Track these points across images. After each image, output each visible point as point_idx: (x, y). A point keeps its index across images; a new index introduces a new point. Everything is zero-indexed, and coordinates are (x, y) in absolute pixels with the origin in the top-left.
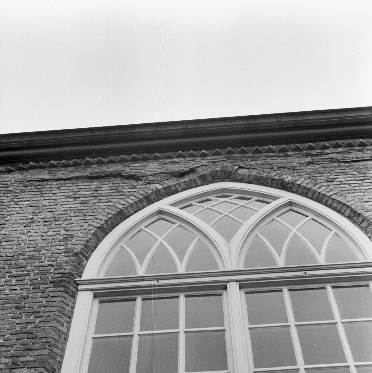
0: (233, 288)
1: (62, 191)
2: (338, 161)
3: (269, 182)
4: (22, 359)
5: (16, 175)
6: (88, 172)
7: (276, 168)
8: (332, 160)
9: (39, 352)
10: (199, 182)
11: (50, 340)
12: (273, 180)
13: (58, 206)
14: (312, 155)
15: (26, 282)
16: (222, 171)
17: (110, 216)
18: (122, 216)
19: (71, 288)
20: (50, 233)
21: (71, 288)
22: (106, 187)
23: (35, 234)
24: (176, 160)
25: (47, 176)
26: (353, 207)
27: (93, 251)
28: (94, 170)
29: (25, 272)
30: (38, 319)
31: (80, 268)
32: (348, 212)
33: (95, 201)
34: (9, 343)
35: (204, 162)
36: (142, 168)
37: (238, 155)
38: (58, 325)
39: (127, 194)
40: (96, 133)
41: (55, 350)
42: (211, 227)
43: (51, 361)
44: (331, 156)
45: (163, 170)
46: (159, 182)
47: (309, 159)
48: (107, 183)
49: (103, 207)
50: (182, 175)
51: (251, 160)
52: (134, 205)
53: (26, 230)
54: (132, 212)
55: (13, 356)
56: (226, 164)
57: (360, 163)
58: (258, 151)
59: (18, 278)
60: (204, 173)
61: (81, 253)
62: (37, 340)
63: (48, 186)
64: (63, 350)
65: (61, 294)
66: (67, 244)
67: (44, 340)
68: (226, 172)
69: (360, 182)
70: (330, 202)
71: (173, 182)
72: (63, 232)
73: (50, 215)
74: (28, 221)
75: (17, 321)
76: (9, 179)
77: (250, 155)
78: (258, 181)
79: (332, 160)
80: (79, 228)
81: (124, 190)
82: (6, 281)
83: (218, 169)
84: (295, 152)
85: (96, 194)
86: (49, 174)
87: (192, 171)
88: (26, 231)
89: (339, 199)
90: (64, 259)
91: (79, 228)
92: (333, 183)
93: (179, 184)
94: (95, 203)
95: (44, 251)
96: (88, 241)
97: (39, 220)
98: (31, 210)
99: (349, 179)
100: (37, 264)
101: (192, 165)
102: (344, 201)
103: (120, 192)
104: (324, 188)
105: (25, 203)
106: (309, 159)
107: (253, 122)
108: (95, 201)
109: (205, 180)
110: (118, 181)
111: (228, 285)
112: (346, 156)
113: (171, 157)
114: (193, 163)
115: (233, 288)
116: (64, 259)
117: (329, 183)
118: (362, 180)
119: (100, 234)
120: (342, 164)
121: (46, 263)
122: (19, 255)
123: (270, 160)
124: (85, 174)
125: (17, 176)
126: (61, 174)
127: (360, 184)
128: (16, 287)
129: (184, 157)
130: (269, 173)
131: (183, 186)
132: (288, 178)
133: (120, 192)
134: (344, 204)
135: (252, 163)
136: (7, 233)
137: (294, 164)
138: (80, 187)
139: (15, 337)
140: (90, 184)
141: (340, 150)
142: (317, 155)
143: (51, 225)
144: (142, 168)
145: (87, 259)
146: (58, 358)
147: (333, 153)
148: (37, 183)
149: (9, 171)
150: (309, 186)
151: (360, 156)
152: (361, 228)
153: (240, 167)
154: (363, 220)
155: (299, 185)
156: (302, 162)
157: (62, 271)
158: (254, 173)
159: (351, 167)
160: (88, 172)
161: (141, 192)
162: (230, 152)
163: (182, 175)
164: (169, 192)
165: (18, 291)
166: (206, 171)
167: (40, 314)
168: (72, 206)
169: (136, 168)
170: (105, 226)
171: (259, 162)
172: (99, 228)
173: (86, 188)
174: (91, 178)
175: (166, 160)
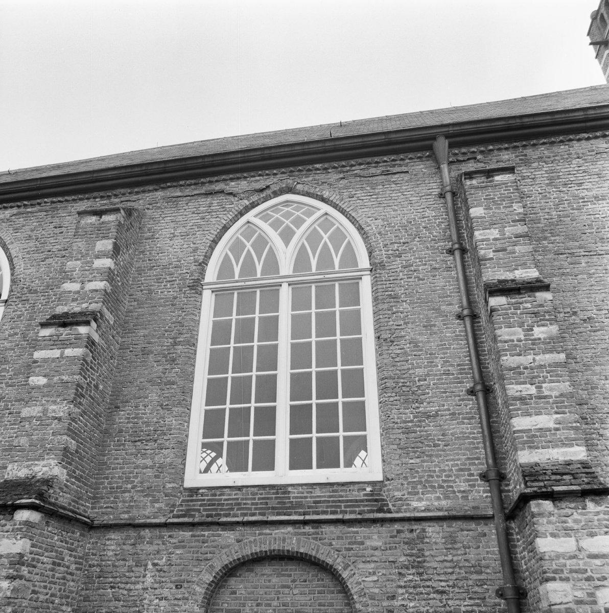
0: (285, 286)
1: (190, 207)
2: (360, 176)
3: (315, 196)
4: (178, 340)
5: (160, 193)
6: (203, 190)
7: (320, 183)
8: (356, 176)
9: (186, 335)
10: (272, 196)
11: (190, 327)
12: (317, 195)
13: (188, 222)
14: (344, 172)
15: (175, 286)
16: (286, 187)
17: (218, 230)
18: (225, 229)
19: (199, 288)
20: (185, 246)
21: (199, 288)
22: (215, 201)
23: (176, 247)
24: (258, 178)
25: (179, 194)
26: (360, 222)
27: (210, 258)
28: (208, 188)
29: (174, 279)
30: (184, 313)
31: (202, 273)
32: (357, 225)
33: (209, 217)
34: (170, 329)
35: (275, 180)
36: (237, 186)
37: (297, 173)
38: (193, 317)
39: (228, 209)
40: (206, 160)
41: (194, 333)
42: (200, 446)
43: (192, 340)
44: (356, 172)
45: (250, 188)
46: (248, 198)
47: (341, 176)
48: (215, 198)
49: (214, 222)
50: (262, 190)
51: (306, 177)
52: (233, 220)
53: (171, 243)
54: (231, 224)
55: (173, 338)
56: (289, 181)
57: (374, 178)
58: (309, 170)
59: (171, 283)
60: (275, 189)
61: (203, 262)
62: (184, 328)
63: (183, 202)
64: (198, 331)
65: (193, 295)
66: (195, 255)
67: (187, 328)
68: (289, 188)
69: (370, 197)
70: (348, 216)
71: (255, 198)
72: (192, 245)
73: (184, 230)
74: (172, 236)
75: (173, 314)
76: (156, 196)
77: (304, 172)
78: (308, 194)
79: (356, 176)
80: (201, 242)
81: (227, 206)
82: (165, 286)
83: (284, 186)
84: (333, 170)
85: (209, 211)
86: (180, 191)
87: (268, 187)
88: (171, 244)
89: (353, 215)
90: (194, 267)
91: (201, 242)
92: (353, 199)
93: (260, 199)
94: (209, 218)
95: (183, 262)
96: (206, 253)
97: (178, 234)
98: (172, 225)
99: (363, 195)
100: (180, 272)
101: (268, 183)
102: (356, 217)
103: (224, 208)
104: (346, 204)
105: (169, 218)
106: (341, 176)
107: (307, 147)
108: (209, 217)
109: (276, 194)
110: (222, 197)
111: (282, 284)
112: (365, 173)
113: (254, 176)
114: (268, 180)
115: (285, 286)
116: (194, 267)
117: (350, 199)
118: (371, 195)
119: (213, 245)
120: (362, 179)
121: (185, 271)
122: (170, 264)
123: (317, 177)
124: (203, 191)
125: (160, 194)
126: (188, 191)
127: (369, 199)
128: (170, 290)
129: (262, 176)
130: (316, 188)
131: (262, 200)
132: (326, 194)
133: (224, 208)
134: (356, 220)
135: (306, 180)
136: (161, 246)
137: (332, 180)
138: (200, 203)
139: (173, 325)
140: (205, 200)
141: (362, 167)
142: (347, 172)
143: (185, 238)
144: (237, 186)
145: (207, 265)
146: (196, 337)
147: (357, 170)
148: (174, 199)
149: (156, 190)
150: (337, 203)
151: (374, 172)
152: (363, 238)
153: (298, 183)
154: (364, 233)
155: (332, 201)
156: (337, 178)
157: (193, 278)
158: (306, 189)
159: (367, 182)
160: (203, 190)
161: (237, 208)
162: (292, 172)
163: (262, 190)
164: (254, 205)
165: (172, 293)
166: (275, 188)
167: (184, 310)
168: (196, 221)
169: (233, 186)
170: (216, 239)
171: (310, 179)
172: (212, 241)
173: (204, 202)
174: (207, 194)
175: (252, 179)
